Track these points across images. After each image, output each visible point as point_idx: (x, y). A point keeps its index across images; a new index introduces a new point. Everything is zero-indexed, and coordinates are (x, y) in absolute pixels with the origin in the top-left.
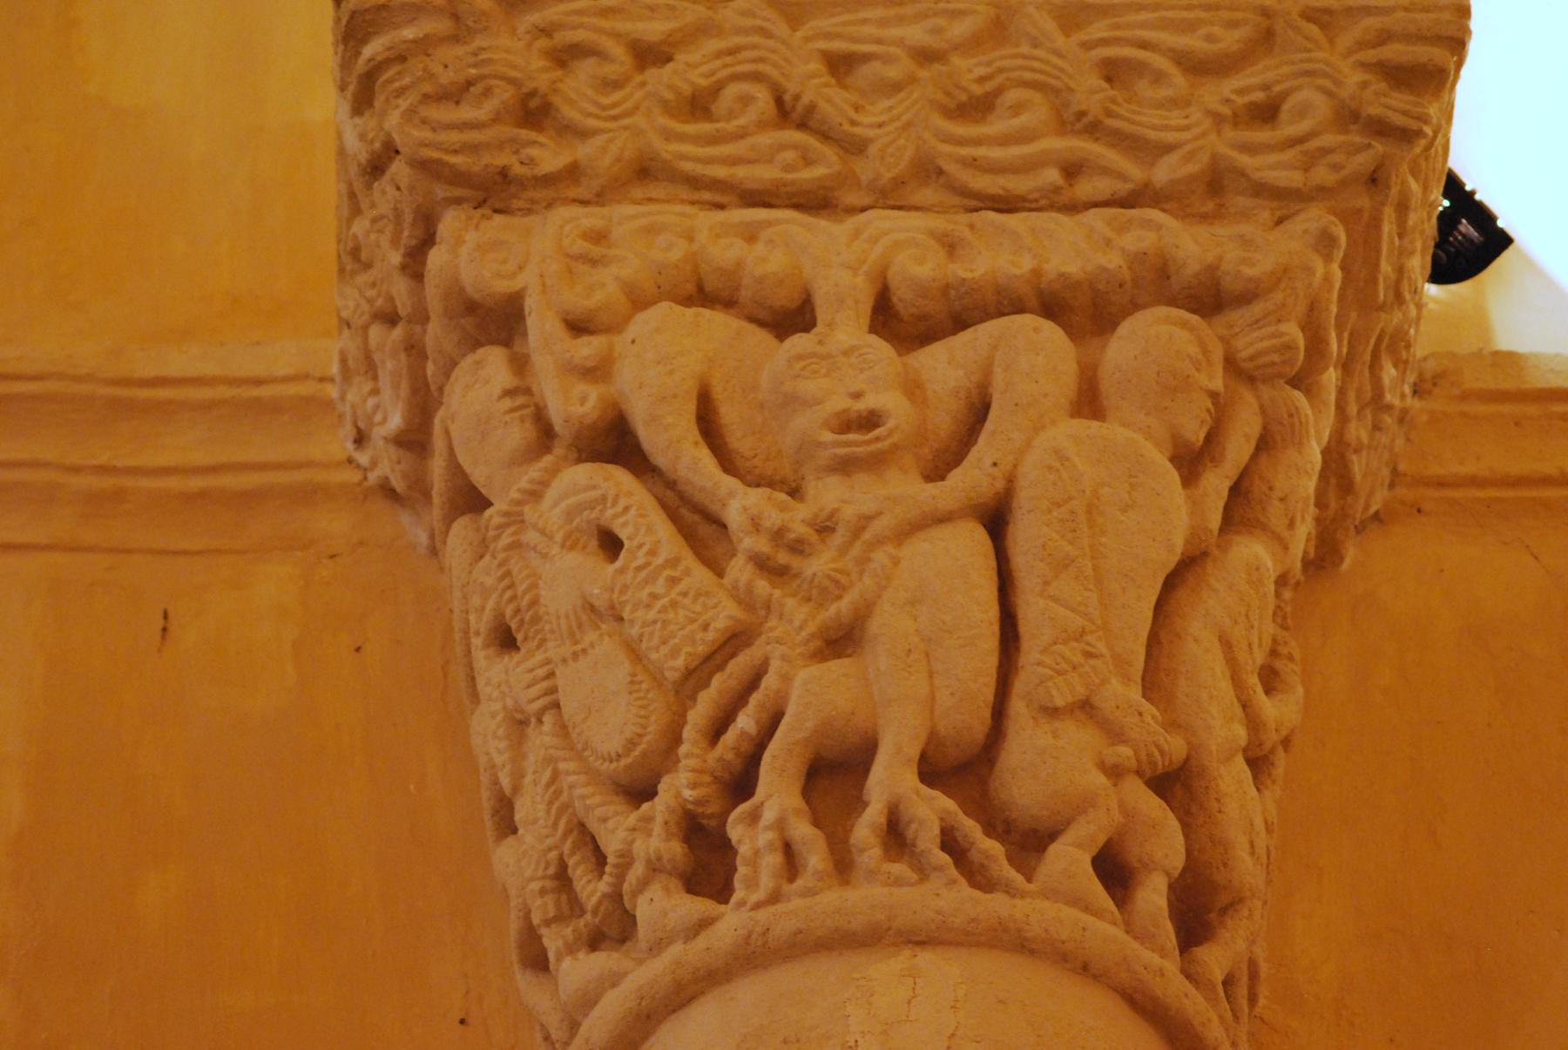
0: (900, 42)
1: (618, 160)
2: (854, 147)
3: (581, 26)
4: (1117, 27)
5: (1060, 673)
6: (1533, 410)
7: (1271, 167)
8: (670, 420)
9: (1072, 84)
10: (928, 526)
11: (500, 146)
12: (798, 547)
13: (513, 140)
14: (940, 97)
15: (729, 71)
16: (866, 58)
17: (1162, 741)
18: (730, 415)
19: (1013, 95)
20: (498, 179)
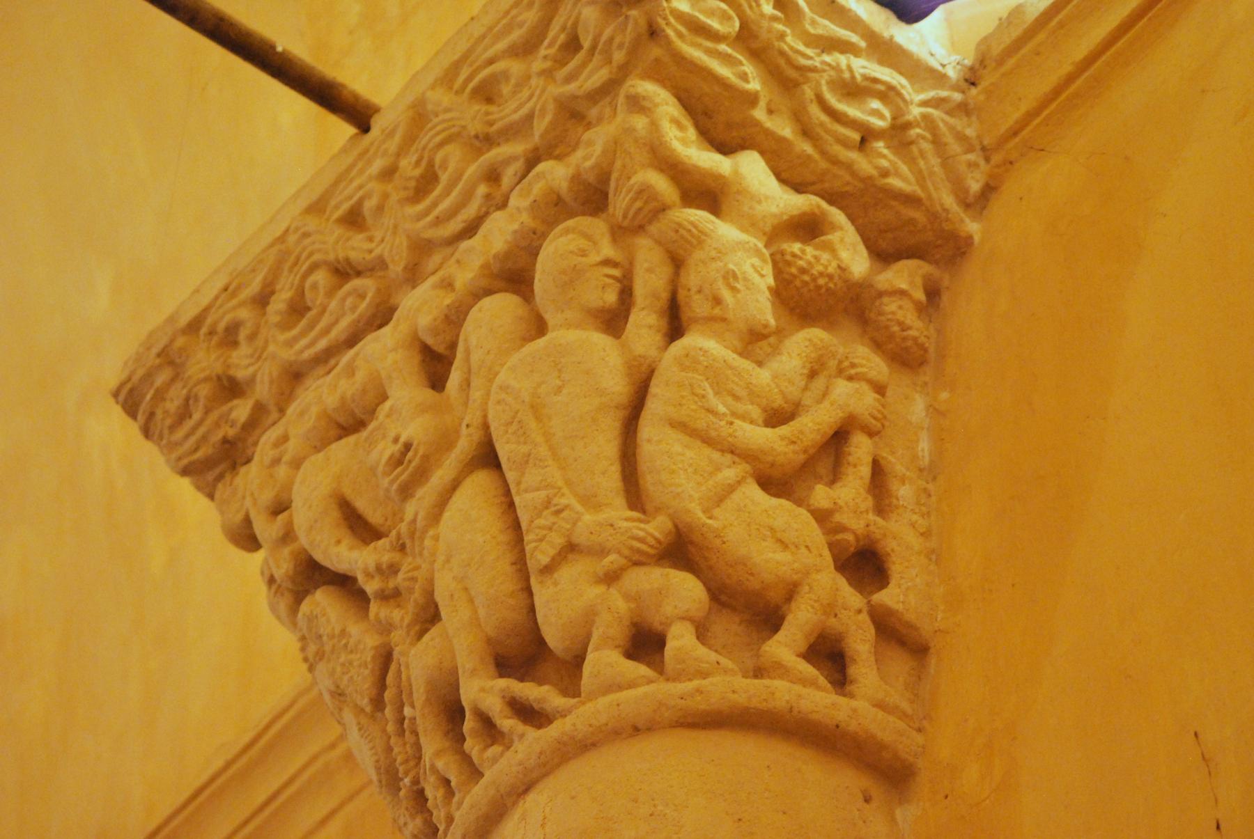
0: (370, 178)
1: (271, 382)
2: (379, 265)
3: (225, 314)
4: (471, 65)
5: (541, 540)
6: (1041, 36)
7: (589, 77)
8: (319, 538)
9: (463, 123)
10: (448, 499)
11: (217, 425)
12: (393, 569)
13: (221, 417)
14: (403, 194)
15: (298, 277)
16: (360, 203)
17: (636, 532)
18: (362, 504)
19: (438, 159)
20: (227, 446)
